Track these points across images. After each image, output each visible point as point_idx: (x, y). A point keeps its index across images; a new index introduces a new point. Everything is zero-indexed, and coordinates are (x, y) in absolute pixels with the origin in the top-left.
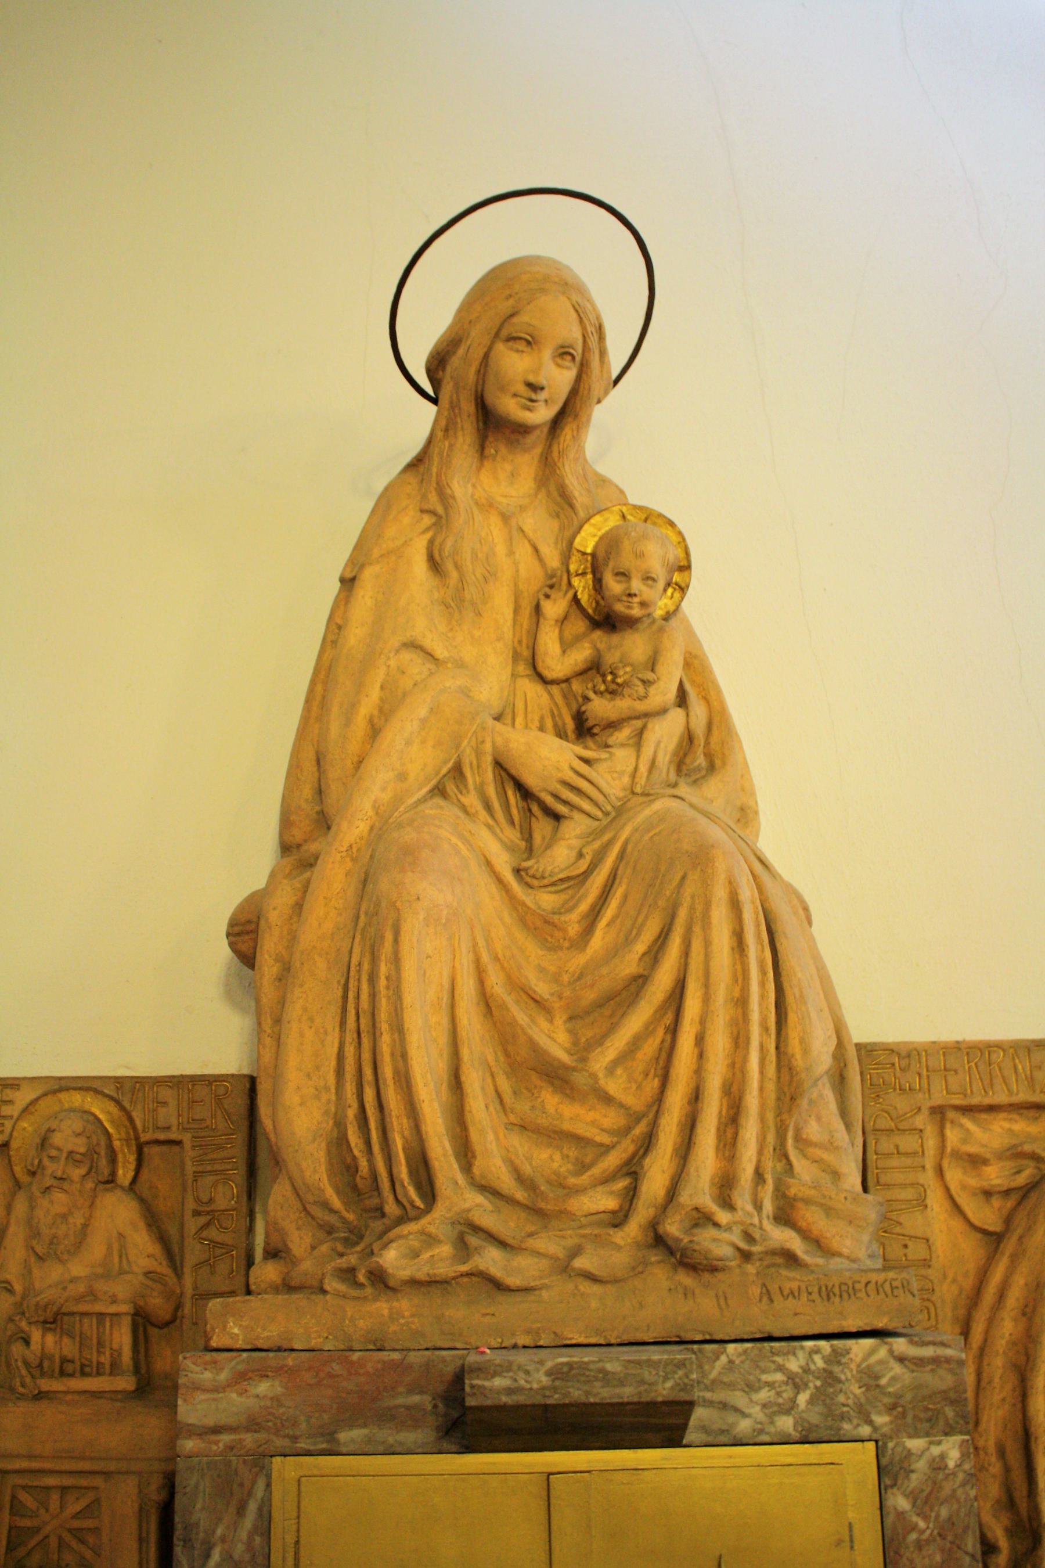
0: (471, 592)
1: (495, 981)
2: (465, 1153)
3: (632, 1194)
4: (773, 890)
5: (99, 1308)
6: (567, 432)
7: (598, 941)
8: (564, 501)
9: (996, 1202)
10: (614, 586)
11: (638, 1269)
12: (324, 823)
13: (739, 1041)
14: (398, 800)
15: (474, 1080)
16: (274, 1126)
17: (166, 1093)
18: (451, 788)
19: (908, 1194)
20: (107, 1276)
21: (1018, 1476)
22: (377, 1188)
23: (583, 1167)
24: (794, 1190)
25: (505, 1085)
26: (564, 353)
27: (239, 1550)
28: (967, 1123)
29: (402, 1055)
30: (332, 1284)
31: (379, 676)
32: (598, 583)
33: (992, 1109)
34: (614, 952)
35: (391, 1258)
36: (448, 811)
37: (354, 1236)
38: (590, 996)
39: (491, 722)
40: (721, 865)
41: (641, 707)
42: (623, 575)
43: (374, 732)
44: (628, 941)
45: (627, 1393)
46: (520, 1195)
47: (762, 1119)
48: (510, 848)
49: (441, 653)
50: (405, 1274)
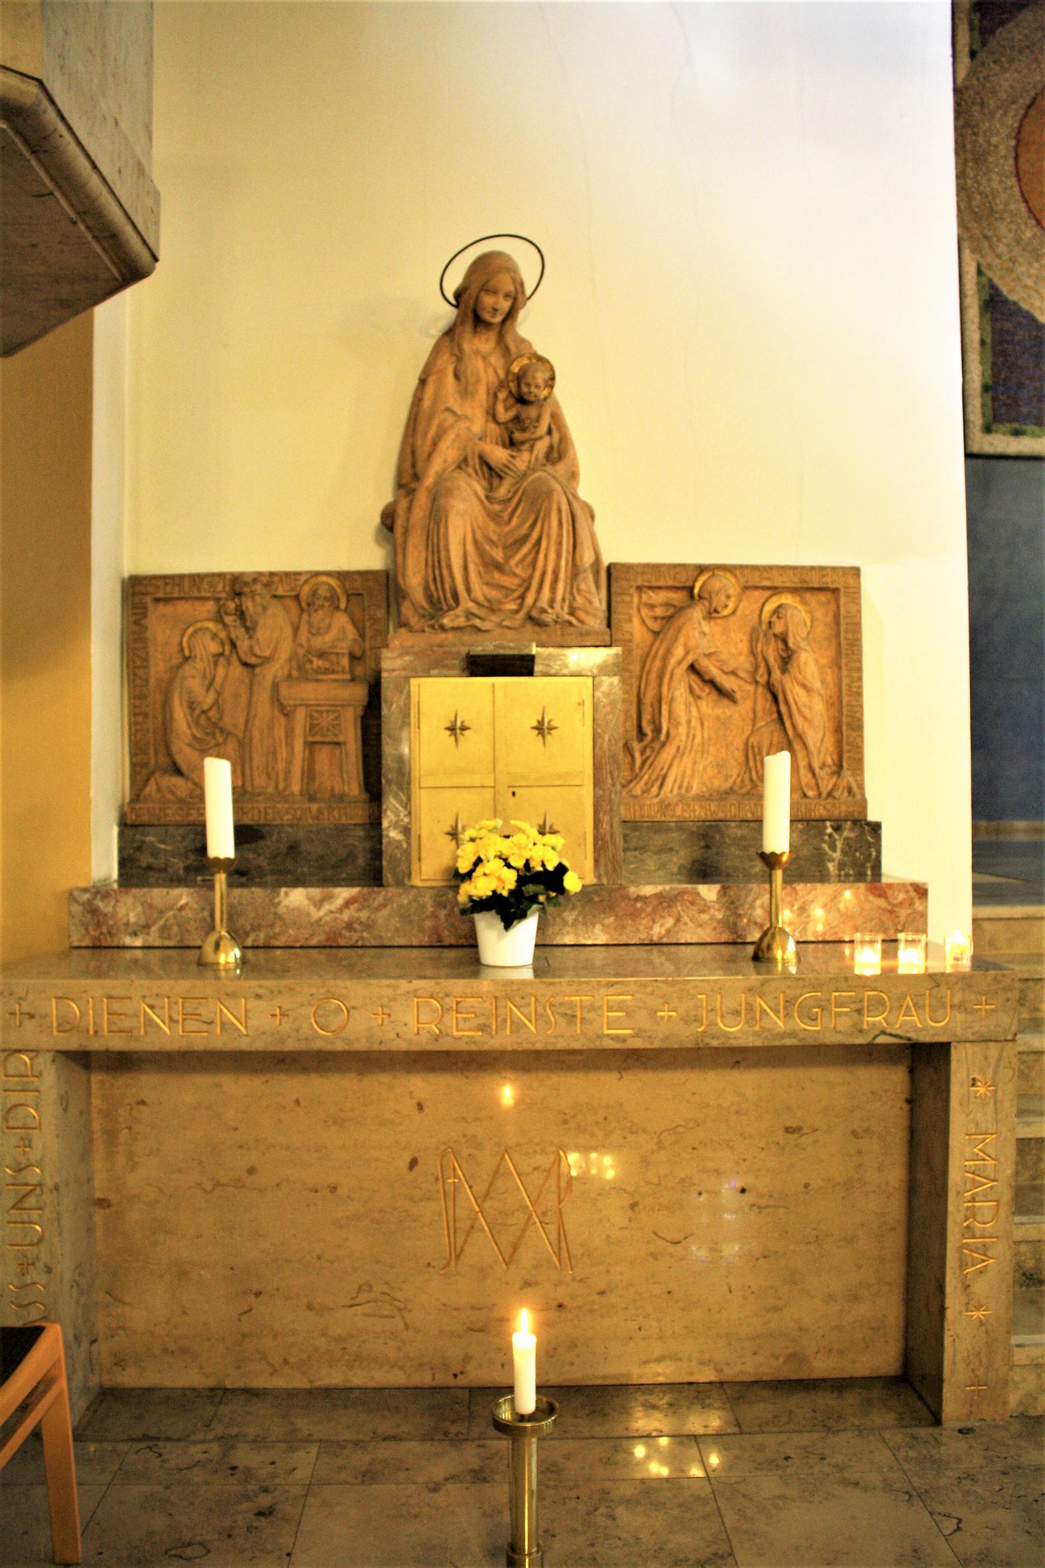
0: (470, 389)
1: (479, 536)
2: (469, 590)
3: (521, 605)
4: (576, 506)
5: (338, 651)
6: (509, 322)
7: (514, 522)
8: (506, 350)
9: (659, 622)
10: (525, 389)
11: (522, 626)
12: (417, 477)
13: (559, 556)
14: (444, 470)
15: (472, 568)
16: (247, 722)
17: (357, 577)
18: (463, 466)
19: (626, 617)
20: (338, 640)
21: (657, 711)
22: (440, 602)
23: (507, 596)
24: (575, 605)
25: (481, 569)
26: (507, 296)
27: (401, 703)
28: (651, 593)
29: (448, 558)
30: (427, 629)
31: (436, 422)
32: (519, 386)
33: (659, 588)
34: (520, 526)
35: (446, 621)
36: (463, 475)
37: (432, 617)
38: (511, 540)
39: (477, 442)
40: (555, 498)
41: (533, 436)
42: (528, 385)
43: (435, 444)
44: (523, 523)
45: (516, 652)
46: (486, 604)
47: (566, 581)
48: (484, 488)
49: (459, 412)
50: (451, 625)
